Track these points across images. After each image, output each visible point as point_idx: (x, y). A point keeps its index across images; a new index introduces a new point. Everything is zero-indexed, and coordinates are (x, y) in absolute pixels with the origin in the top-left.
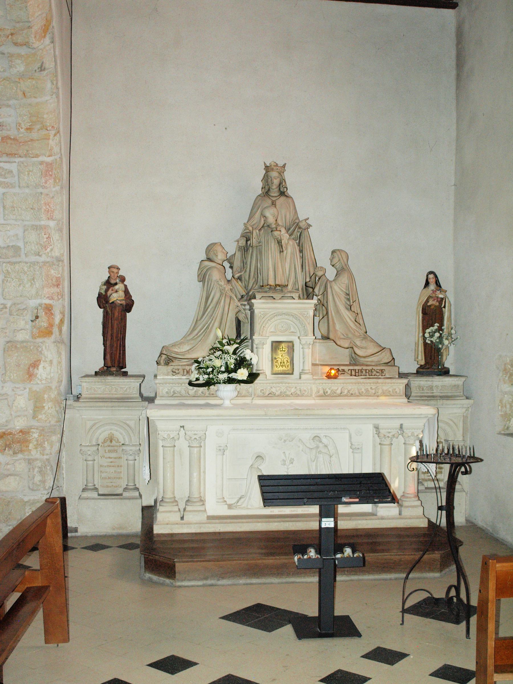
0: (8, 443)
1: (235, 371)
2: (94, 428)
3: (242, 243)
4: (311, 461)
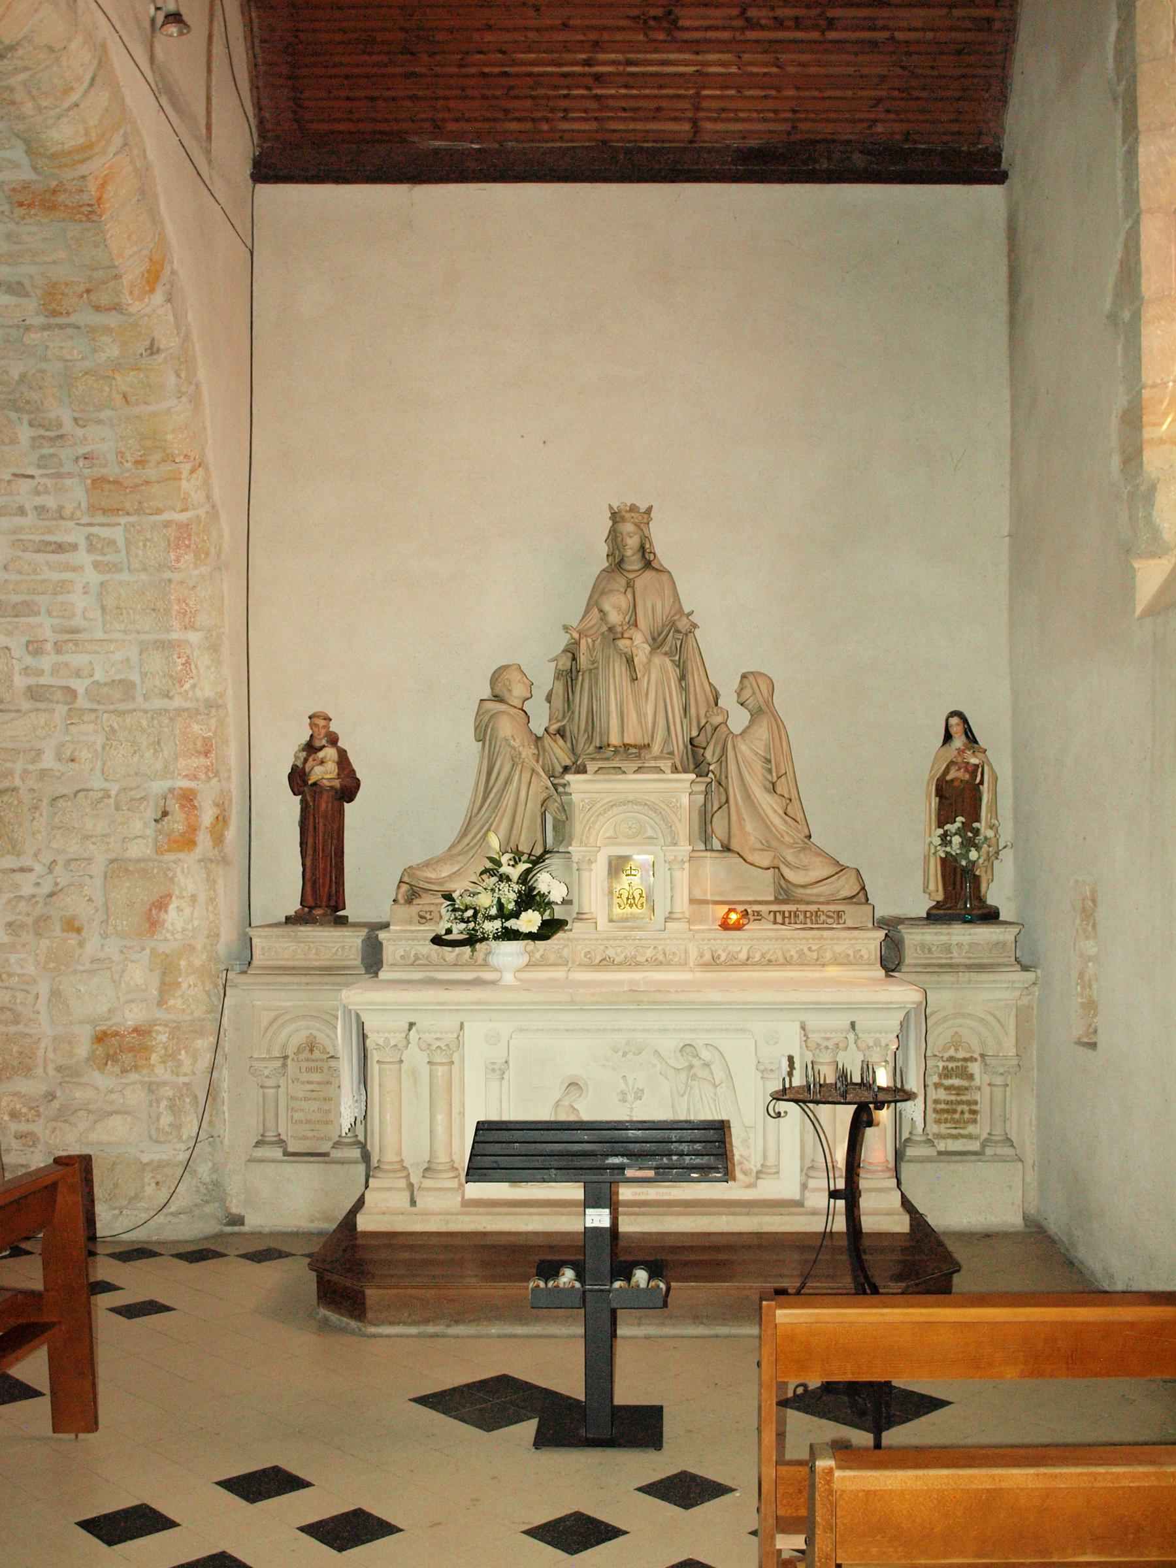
0: (111, 1052)
1: (516, 915)
2: (275, 1026)
3: (564, 664)
4: (678, 1093)
